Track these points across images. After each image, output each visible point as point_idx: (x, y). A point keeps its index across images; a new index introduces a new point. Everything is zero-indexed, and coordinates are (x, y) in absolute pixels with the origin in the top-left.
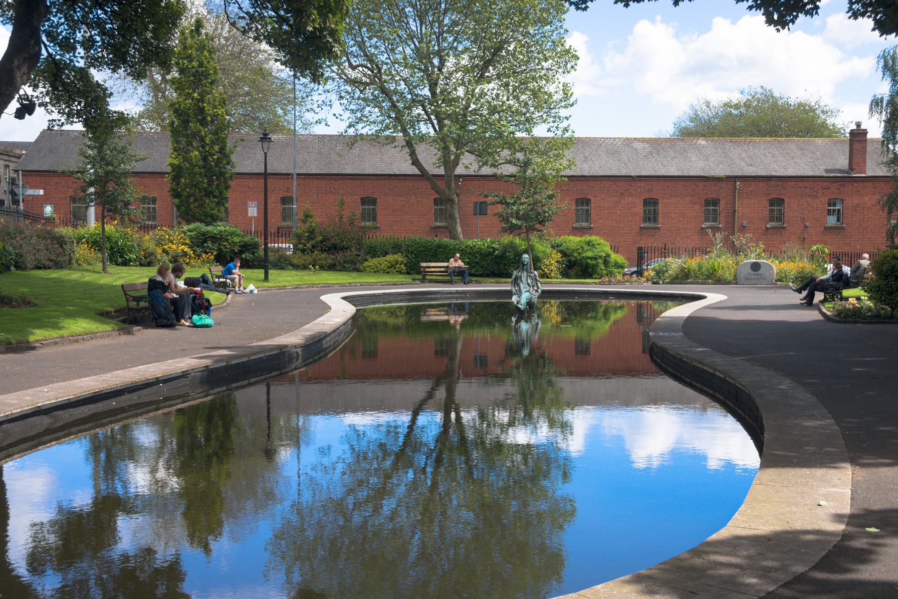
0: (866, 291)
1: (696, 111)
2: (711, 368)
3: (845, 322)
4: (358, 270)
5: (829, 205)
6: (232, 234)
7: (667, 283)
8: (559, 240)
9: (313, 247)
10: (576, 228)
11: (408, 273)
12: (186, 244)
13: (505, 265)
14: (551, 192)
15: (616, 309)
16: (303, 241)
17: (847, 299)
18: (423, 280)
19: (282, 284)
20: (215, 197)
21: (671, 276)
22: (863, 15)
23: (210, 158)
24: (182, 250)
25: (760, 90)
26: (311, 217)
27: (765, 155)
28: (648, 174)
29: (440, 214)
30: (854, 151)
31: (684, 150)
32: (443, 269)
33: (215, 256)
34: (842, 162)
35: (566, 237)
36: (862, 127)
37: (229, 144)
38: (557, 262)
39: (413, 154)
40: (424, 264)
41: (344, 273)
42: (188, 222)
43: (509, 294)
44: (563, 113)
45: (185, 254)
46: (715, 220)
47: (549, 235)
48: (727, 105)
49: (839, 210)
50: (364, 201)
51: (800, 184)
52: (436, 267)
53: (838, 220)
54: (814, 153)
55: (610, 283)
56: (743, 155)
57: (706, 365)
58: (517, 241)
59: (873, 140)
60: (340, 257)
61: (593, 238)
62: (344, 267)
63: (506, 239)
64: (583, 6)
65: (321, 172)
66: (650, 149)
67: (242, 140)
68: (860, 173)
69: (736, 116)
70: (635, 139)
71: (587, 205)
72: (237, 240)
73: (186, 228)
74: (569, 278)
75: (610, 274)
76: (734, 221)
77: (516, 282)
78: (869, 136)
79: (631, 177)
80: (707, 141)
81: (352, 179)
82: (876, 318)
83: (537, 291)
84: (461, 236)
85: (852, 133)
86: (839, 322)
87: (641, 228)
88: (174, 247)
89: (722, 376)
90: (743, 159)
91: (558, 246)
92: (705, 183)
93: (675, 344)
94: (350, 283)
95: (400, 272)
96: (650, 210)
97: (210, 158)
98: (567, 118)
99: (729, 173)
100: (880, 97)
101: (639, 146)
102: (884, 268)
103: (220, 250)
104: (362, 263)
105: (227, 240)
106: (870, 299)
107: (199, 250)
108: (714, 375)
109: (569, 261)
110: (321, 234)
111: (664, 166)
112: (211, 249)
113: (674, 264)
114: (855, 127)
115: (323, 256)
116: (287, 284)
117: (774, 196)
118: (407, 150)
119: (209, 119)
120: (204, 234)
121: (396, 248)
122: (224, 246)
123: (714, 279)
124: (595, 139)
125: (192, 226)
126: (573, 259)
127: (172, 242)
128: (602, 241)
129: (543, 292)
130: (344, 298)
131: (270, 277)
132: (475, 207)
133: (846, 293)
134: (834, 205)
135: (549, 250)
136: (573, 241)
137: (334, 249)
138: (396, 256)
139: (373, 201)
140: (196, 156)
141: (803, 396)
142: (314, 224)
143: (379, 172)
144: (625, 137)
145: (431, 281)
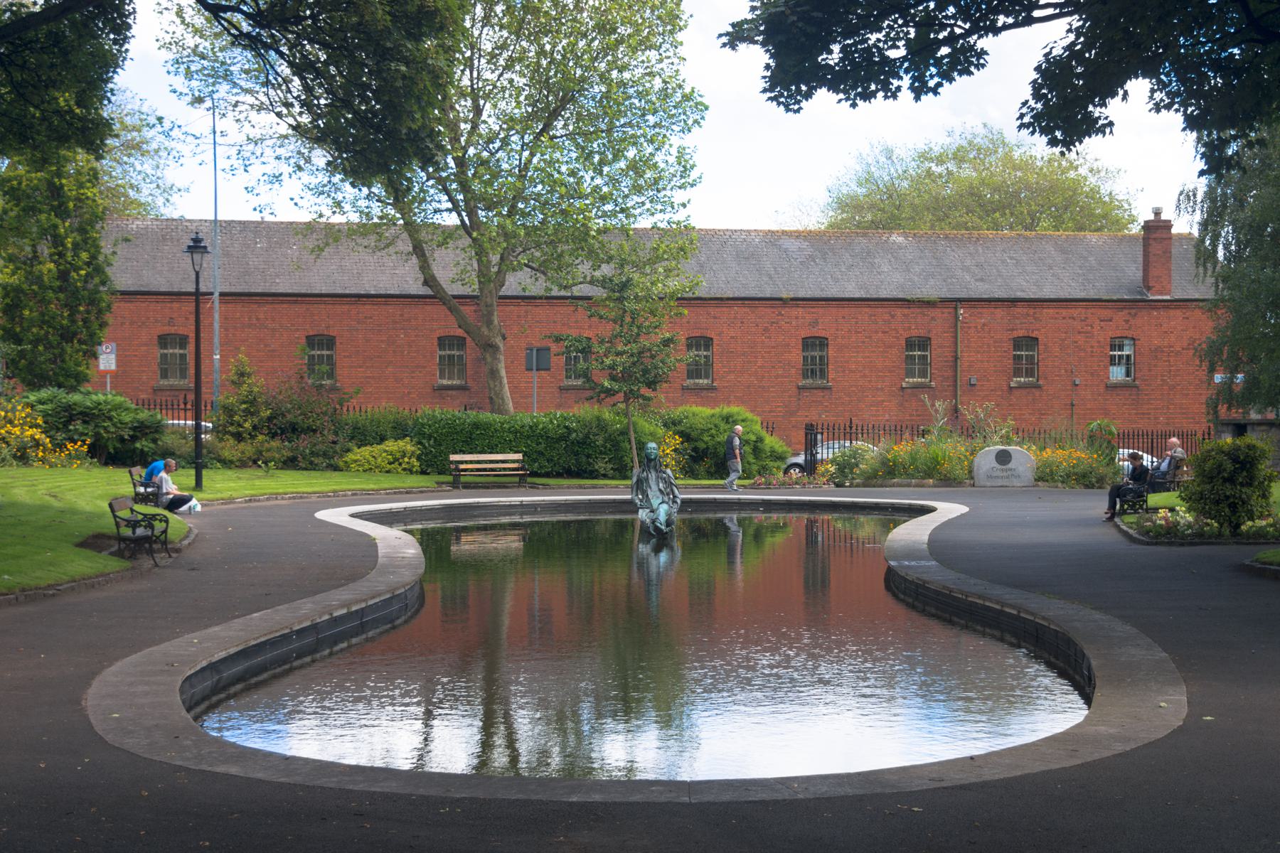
0: (1183, 499)
1: (869, 165)
2: (997, 603)
3: (1156, 544)
4: (336, 468)
5: (1113, 348)
6: (118, 407)
7: (858, 486)
8: (678, 412)
9: (255, 427)
10: (688, 388)
11: (423, 473)
12: (37, 426)
13: (588, 456)
14: (668, 335)
15: (776, 528)
16: (236, 418)
17: (1156, 510)
18: (455, 485)
19: (226, 495)
20: (81, 342)
21: (863, 472)
22: (1168, 107)
23: (74, 274)
24: (32, 437)
25: (982, 131)
26: (249, 375)
27: (1003, 262)
28: (809, 294)
29: (448, 364)
30: (1152, 258)
31: (868, 253)
32: (516, 465)
33: (89, 447)
34: (1134, 272)
35: (688, 408)
36: (1163, 217)
37: (106, 247)
38: (675, 450)
39: (425, 266)
40: (454, 457)
41: (313, 473)
42: (33, 386)
43: (630, 507)
44: (679, 196)
45: (37, 444)
46: (923, 374)
47: (659, 405)
48: (924, 156)
49: (1128, 356)
50: (312, 341)
51: (1064, 312)
52: (471, 462)
53: (1128, 374)
54: (1085, 258)
55: (768, 486)
56: (968, 263)
57: (990, 600)
58: (607, 415)
59: (1181, 237)
60: (304, 444)
61: (734, 409)
62: (311, 463)
63: (585, 411)
64: (796, 107)
65: (233, 290)
66: (809, 251)
67: (127, 240)
68: (1161, 294)
69: (940, 176)
70: (784, 232)
71: (707, 348)
72: (127, 418)
73: (32, 397)
74: (696, 478)
75: (763, 470)
76: (955, 376)
77: (640, 486)
78: (1174, 231)
79: (780, 299)
80: (906, 237)
81: (289, 302)
82: (1200, 538)
83: (674, 502)
84: (511, 406)
85: (1147, 226)
86: (1148, 544)
87: (799, 388)
88: (17, 431)
89: (1015, 612)
90: (966, 269)
91: (674, 423)
92: (906, 311)
93: (932, 572)
94: (334, 491)
95: (410, 471)
96: (813, 358)
97: (74, 274)
98: (684, 205)
99: (945, 293)
100: (1191, 188)
101: (791, 245)
102: (1208, 466)
103: (97, 436)
104: (342, 456)
105: (110, 419)
106: (1189, 510)
107: (60, 436)
108: (1001, 612)
109: (695, 449)
110: (267, 404)
111: (837, 280)
112: (82, 434)
113: (870, 451)
114: (1152, 217)
115: (273, 443)
116: (235, 494)
117: (1021, 333)
118: (414, 259)
119: (71, 205)
120: (68, 407)
121: (400, 431)
122: (105, 428)
123: (946, 479)
124: (715, 233)
125: (44, 393)
126: (702, 446)
127: (11, 422)
128: (749, 415)
129: (684, 502)
130: (352, 516)
131: (205, 482)
132: (529, 357)
133: (1153, 499)
134: (1121, 348)
135: (661, 431)
136: (700, 413)
137: (293, 430)
138: (401, 443)
139: (330, 342)
140: (50, 271)
141: (1122, 629)
142: (256, 389)
143: (340, 291)
144: (766, 228)
145: (467, 486)
